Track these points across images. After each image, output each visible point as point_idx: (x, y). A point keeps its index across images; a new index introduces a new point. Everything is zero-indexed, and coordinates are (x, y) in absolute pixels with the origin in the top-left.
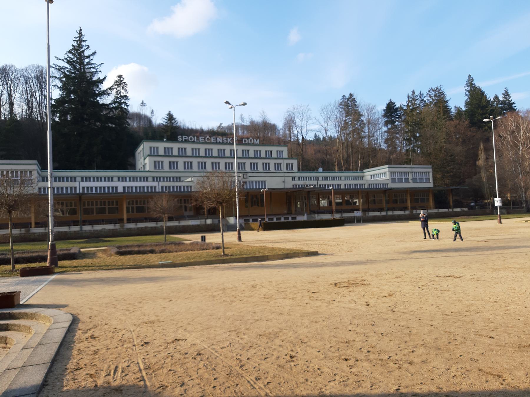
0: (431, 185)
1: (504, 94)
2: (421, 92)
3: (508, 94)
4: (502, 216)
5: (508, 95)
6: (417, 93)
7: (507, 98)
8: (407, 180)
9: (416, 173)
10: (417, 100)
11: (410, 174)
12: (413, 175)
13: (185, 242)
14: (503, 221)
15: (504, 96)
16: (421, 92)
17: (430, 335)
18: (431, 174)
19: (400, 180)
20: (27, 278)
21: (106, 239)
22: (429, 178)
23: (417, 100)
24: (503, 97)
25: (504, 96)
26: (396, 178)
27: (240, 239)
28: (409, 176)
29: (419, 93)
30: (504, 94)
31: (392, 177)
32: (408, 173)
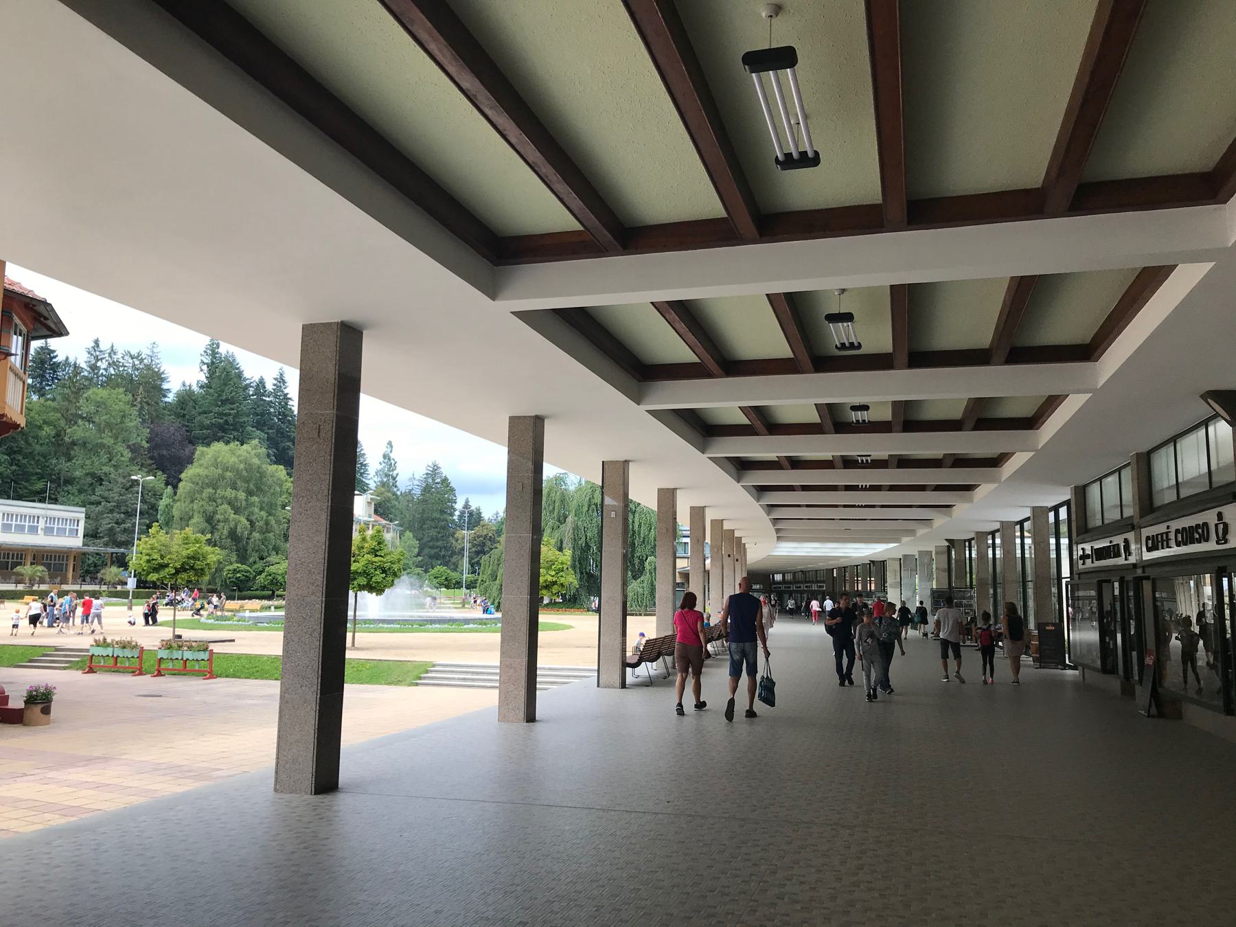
0: (77, 542)
1: (276, 379)
2: (112, 346)
3: (283, 380)
4: (134, 601)
5: (284, 382)
6: (104, 346)
7: (281, 387)
8: (33, 530)
9: (53, 519)
10: (101, 359)
11: (41, 519)
12: (46, 521)
13: (759, 642)
14: (133, 607)
15: (275, 382)
16: (112, 346)
17: (732, 832)
18: (82, 524)
19: (20, 529)
20: (905, 206)
21: (1226, 593)
22: (77, 530)
23: (101, 359)
24: (275, 385)
25: (275, 382)
26: (25, 525)
27: (1000, 584)
28: (38, 522)
29: (64, 359)
30: (276, 379)
31: (5, 522)
32: (38, 517)
